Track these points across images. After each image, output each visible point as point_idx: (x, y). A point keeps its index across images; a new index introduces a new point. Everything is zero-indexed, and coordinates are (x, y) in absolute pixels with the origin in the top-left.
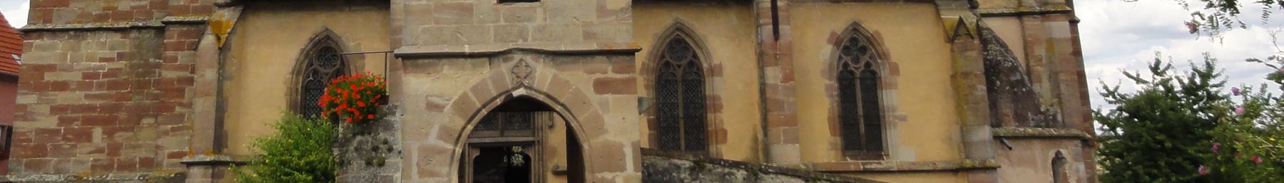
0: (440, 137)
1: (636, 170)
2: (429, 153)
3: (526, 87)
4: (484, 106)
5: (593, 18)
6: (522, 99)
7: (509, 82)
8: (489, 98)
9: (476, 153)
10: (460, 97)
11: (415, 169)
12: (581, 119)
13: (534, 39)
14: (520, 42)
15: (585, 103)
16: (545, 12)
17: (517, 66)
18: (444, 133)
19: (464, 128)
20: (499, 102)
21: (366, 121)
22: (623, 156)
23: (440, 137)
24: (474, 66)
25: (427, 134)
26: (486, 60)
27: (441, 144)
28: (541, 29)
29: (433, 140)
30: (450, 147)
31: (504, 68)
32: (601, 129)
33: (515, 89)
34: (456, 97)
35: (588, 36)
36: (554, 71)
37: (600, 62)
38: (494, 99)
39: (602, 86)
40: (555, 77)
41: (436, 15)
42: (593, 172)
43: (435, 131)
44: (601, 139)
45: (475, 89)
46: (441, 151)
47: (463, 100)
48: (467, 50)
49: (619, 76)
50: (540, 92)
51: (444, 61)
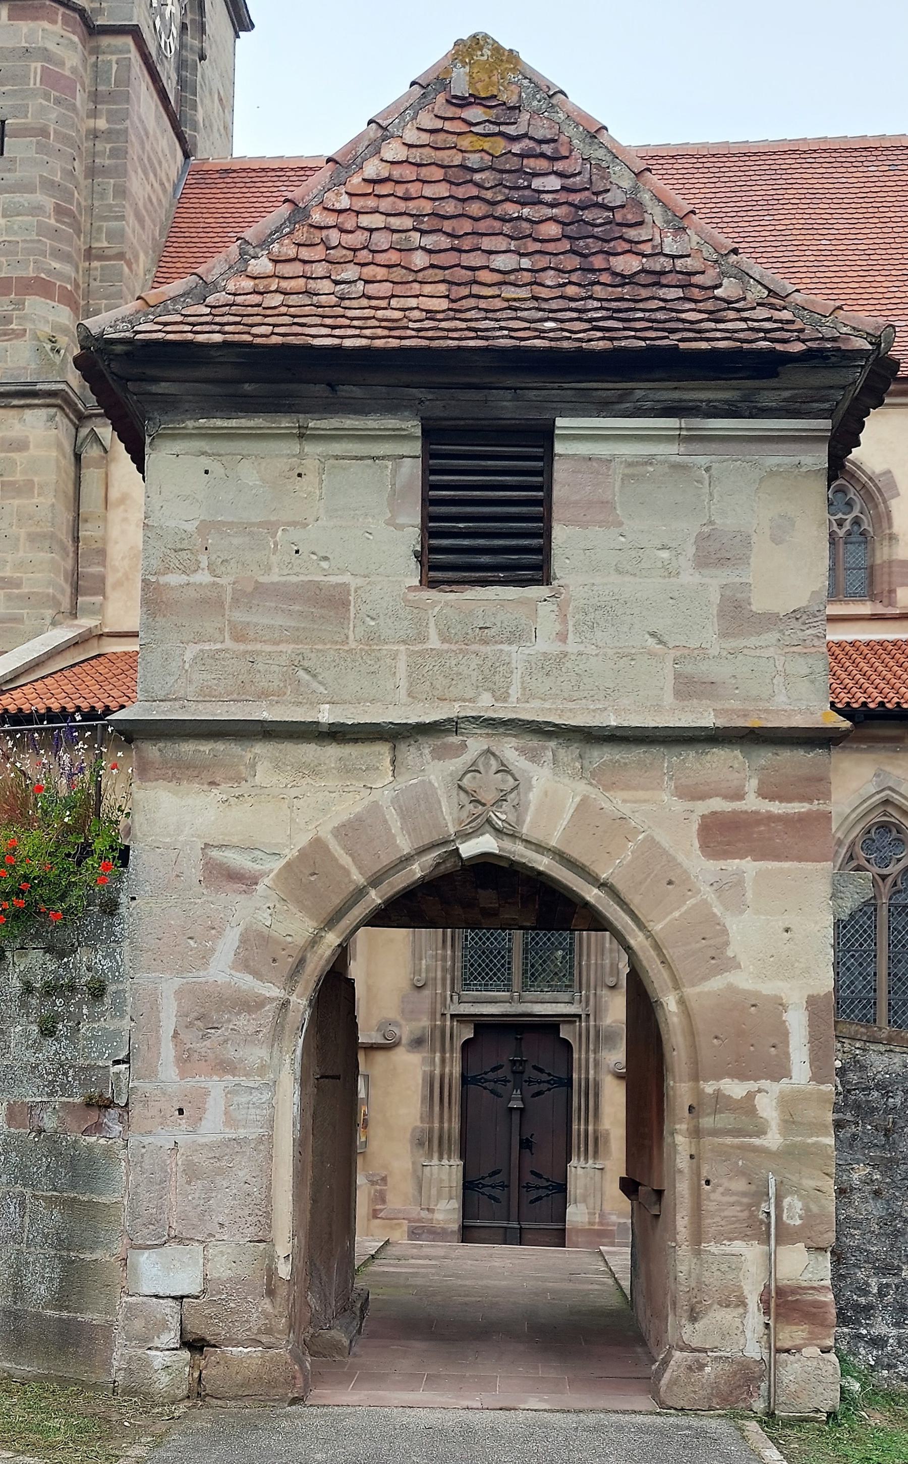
0: (244, 964)
1: (818, 1077)
2: (208, 1013)
3: (498, 832)
4: (375, 882)
5: (708, 635)
6: (487, 869)
7: (449, 815)
8: (386, 860)
9: (468, 1033)
10: (303, 854)
11: (168, 1051)
12: (405, 845)
13: (528, 695)
14: (486, 700)
15: (675, 881)
16: (563, 618)
17: (473, 769)
18: (256, 949)
19: (314, 941)
20: (417, 871)
21: (863, 1111)
22: (783, 1034)
23: (244, 964)
24: (346, 770)
25: (205, 957)
26: (383, 750)
27: (247, 982)
28: (550, 665)
29: (221, 970)
30: (274, 992)
31: (433, 770)
32: (718, 959)
33: (466, 836)
34: (290, 853)
35: (688, 687)
36: (582, 787)
37: (723, 762)
38: (407, 860)
39: (724, 835)
40: (584, 804)
41: (239, 616)
42: (696, 1077)
43: (230, 941)
44: (716, 984)
45: (349, 831)
46: (250, 1005)
47: (314, 858)
48: (326, 715)
49: (776, 808)
50: (540, 848)
51: (260, 749)
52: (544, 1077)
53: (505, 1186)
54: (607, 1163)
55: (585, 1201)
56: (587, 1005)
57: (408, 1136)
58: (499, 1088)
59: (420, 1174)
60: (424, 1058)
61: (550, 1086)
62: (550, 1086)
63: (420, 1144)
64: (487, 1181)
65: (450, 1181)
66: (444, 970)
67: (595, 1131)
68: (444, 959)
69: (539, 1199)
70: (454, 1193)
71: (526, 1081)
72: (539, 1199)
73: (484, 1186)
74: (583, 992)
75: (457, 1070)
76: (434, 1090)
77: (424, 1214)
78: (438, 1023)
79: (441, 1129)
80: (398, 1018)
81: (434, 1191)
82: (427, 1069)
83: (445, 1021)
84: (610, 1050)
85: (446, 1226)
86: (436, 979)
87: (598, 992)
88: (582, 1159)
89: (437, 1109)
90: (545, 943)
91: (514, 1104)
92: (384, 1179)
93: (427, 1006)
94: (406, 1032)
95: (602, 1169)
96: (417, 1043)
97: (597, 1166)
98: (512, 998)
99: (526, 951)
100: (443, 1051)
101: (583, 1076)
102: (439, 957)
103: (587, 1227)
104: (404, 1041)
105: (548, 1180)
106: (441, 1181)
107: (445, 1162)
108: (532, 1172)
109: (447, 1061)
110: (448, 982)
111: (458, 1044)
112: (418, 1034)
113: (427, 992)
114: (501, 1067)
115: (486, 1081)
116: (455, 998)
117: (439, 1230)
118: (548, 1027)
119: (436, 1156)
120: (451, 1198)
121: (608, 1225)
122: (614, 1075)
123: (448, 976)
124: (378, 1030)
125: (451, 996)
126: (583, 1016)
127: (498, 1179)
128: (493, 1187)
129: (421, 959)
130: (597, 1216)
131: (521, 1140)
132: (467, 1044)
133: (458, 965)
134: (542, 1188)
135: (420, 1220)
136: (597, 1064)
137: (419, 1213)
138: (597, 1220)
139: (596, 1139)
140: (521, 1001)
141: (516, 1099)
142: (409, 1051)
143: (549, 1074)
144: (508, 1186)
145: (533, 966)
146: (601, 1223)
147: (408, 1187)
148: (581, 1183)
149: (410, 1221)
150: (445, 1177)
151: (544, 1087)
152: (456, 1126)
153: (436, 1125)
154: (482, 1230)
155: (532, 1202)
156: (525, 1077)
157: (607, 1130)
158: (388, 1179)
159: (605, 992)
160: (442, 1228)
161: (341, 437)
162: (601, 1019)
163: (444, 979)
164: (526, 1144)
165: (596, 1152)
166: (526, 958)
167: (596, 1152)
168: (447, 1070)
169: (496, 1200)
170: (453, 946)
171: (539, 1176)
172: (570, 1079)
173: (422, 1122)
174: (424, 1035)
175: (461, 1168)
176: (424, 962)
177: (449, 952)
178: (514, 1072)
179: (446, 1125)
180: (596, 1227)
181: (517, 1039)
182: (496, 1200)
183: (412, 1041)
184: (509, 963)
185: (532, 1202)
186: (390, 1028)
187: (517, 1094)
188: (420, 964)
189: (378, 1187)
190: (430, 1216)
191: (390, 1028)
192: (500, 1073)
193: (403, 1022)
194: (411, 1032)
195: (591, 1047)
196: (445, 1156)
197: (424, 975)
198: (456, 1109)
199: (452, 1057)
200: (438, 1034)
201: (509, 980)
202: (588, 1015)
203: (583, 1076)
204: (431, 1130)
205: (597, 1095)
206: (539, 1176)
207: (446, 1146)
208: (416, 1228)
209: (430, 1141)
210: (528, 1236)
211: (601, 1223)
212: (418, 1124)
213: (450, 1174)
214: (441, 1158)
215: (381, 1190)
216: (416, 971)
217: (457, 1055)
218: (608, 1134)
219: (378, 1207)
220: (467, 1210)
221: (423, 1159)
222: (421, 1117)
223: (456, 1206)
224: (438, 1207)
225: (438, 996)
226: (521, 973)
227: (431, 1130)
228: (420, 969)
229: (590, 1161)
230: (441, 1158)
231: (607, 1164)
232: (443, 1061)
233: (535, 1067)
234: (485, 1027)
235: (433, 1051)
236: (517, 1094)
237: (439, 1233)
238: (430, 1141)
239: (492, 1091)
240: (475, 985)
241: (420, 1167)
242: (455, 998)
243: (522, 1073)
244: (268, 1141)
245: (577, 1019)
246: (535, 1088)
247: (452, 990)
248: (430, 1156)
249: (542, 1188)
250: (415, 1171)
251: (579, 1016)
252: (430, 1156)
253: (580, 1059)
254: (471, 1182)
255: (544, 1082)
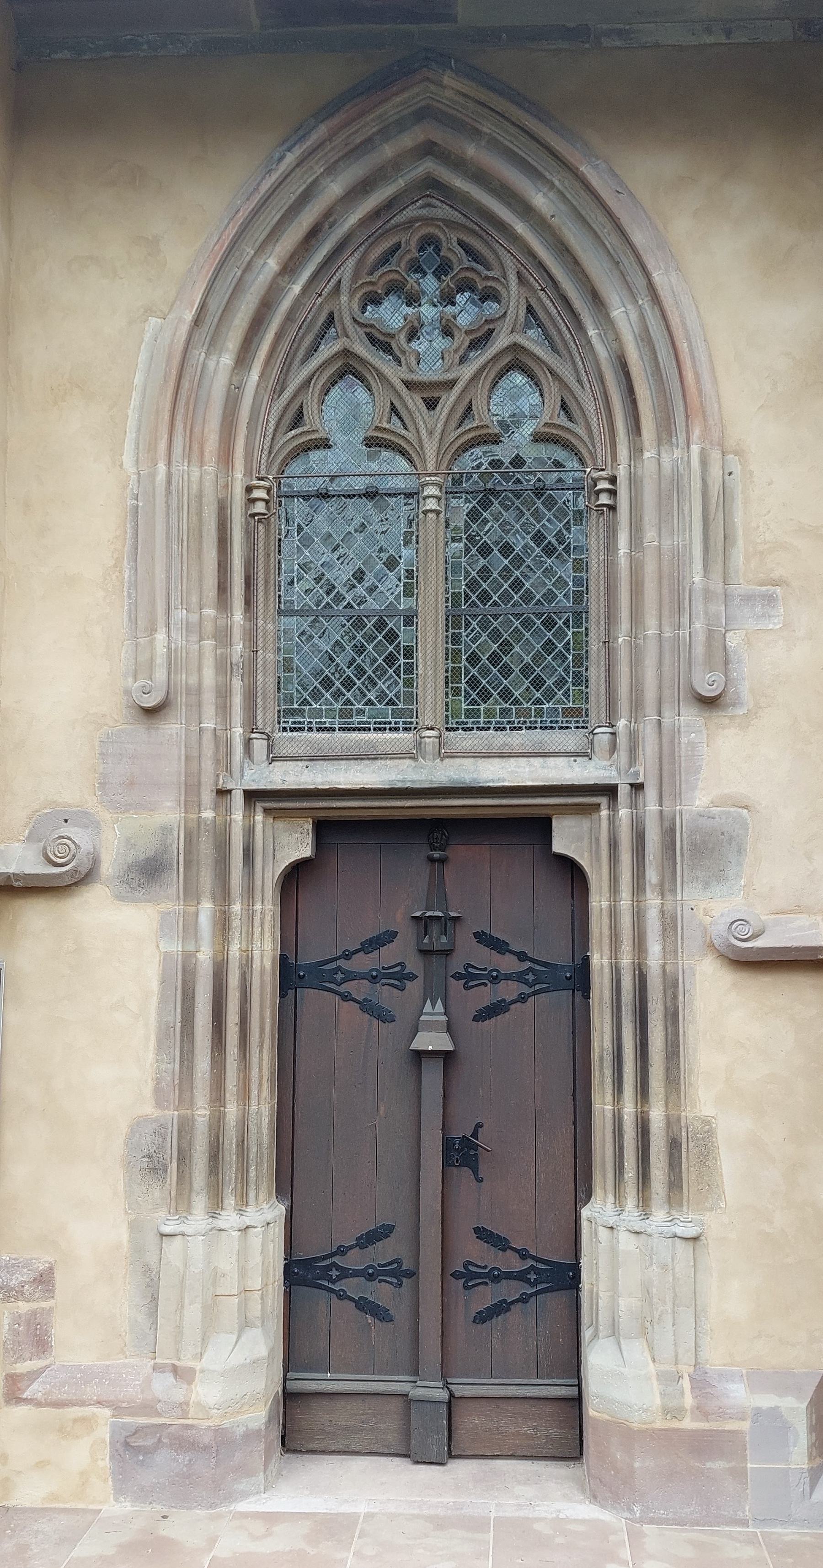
9: (298, 845)
52: (508, 964)
53: (400, 1273)
54: (708, 1218)
55: (645, 1330)
56: (633, 758)
57: (118, 1146)
58: (385, 995)
59: (152, 1259)
60: (165, 915)
61: (527, 990)
62: (527, 990)
63: (153, 1170)
64: (354, 1260)
65: (243, 1273)
66: (223, 666)
67: (671, 1123)
68: (223, 637)
69: (501, 1308)
70: (255, 1309)
71: (457, 976)
72: (501, 1308)
73: (345, 1273)
74: (622, 723)
75: (265, 950)
76: (200, 1011)
77: (163, 1386)
78: (208, 814)
79: (217, 1123)
80: (92, 803)
81: (193, 1313)
82: (175, 947)
83: (229, 810)
84: (706, 885)
85: (226, 1423)
86: (199, 690)
87: (666, 721)
88: (631, 1202)
89: (203, 1063)
90: (506, 597)
91: (427, 1041)
92: (44, 1281)
93: (172, 767)
94: (113, 842)
95: (695, 1239)
96: (148, 872)
97: (679, 1230)
98: (419, 745)
99: (453, 620)
100: (223, 895)
101: (626, 961)
102: (209, 627)
103: (659, 1424)
104: (108, 867)
105: (524, 1255)
106: (216, 1276)
107: (229, 1218)
108: (482, 1234)
109: (236, 923)
110: (237, 700)
111: (269, 876)
112: (146, 848)
113: (172, 728)
114: (391, 936)
115: (350, 977)
116: (259, 746)
117: (206, 1439)
118: (520, 825)
119: (200, 1202)
120: (245, 1324)
121: (722, 1415)
122: (722, 956)
123: (237, 684)
124: (29, 838)
125: (248, 744)
126: (623, 792)
127: (384, 1252)
128: (371, 1277)
129: (153, 630)
130: (686, 1383)
131: (448, 1144)
132: (295, 876)
133: (268, 657)
134: (509, 1276)
135: (148, 1408)
136: (670, 925)
137: (148, 1381)
138: (689, 1401)
139: (674, 1146)
140: (443, 753)
141: (431, 1027)
142: (120, 898)
143: (522, 956)
144: (411, 1274)
145: (473, 659)
146: (701, 1412)
147: (120, 1301)
148: (630, 1278)
149: (118, 1409)
150: (227, 1263)
151: (509, 990)
152: (263, 1108)
153: (202, 1113)
154: (340, 1403)
155: (483, 1317)
156: (457, 964)
157: (706, 1121)
158: (58, 1276)
159: (689, 717)
160: (219, 1431)
161: (374, 758)
162: (677, 795)
163: (223, 695)
164: (461, 1153)
165: (675, 1184)
166: (456, 639)
167: (675, 1184)
168: (235, 950)
169: (379, 1313)
170: (249, 603)
171: (499, 1242)
172: (584, 969)
173: (159, 1104)
174: (165, 849)
175: (278, 1232)
176: (161, 637)
177: (238, 616)
178: (425, 953)
179: (232, 1110)
180: (688, 1424)
181: (431, 860)
182: (379, 1313)
183: (130, 867)
184: (409, 652)
185: (483, 1317)
186: (65, 831)
187: (434, 1012)
188: (152, 642)
189: (23, 1307)
190: (178, 1393)
191: (65, 831)
192: (388, 956)
193: (105, 815)
194: (129, 843)
195: (652, 875)
196: (230, 1201)
197: (160, 675)
198: (263, 1060)
199: (249, 916)
200: (206, 848)
201: (411, 698)
202: (637, 787)
203: (626, 961)
204: (185, 1128)
205: (672, 1017)
206: (499, 1242)
207: (230, 1172)
208: (138, 1431)
209: (184, 1158)
210: (470, 1421)
211: (701, 1412)
212: (149, 1109)
213: (243, 1255)
214: (216, 1205)
215: (34, 1313)
216: (141, 667)
217: (267, 906)
218: (710, 1133)
219: (22, 1367)
220: (297, 1348)
221: (162, 1213)
222: (157, 1090)
223: (262, 1351)
224: (205, 1363)
225: (208, 738)
226: (442, 676)
227: (185, 1128)
228: (152, 660)
229: (659, 1215)
230: (216, 1205)
231: (713, 1223)
232: (223, 924)
233: (482, 938)
234: (346, 828)
235: (191, 893)
236: (434, 1012)
237: (206, 1448)
238: (184, 1158)
239: (366, 1006)
240: (318, 713)
241: (152, 1239)
242: (259, 746)
243: (447, 953)
244: (174, 1027)
245: (603, 801)
246: (485, 995)
247: (251, 726)
248: (181, 1202)
249: (509, 1276)
250: (138, 1249)
251: (610, 791)
252: (181, 1202)
253: (614, 913)
254: (307, 1263)
255: (508, 977)
